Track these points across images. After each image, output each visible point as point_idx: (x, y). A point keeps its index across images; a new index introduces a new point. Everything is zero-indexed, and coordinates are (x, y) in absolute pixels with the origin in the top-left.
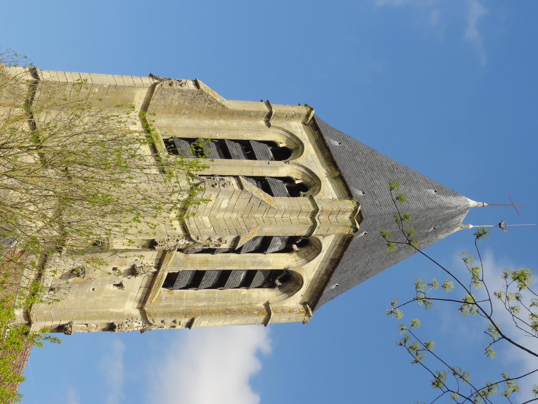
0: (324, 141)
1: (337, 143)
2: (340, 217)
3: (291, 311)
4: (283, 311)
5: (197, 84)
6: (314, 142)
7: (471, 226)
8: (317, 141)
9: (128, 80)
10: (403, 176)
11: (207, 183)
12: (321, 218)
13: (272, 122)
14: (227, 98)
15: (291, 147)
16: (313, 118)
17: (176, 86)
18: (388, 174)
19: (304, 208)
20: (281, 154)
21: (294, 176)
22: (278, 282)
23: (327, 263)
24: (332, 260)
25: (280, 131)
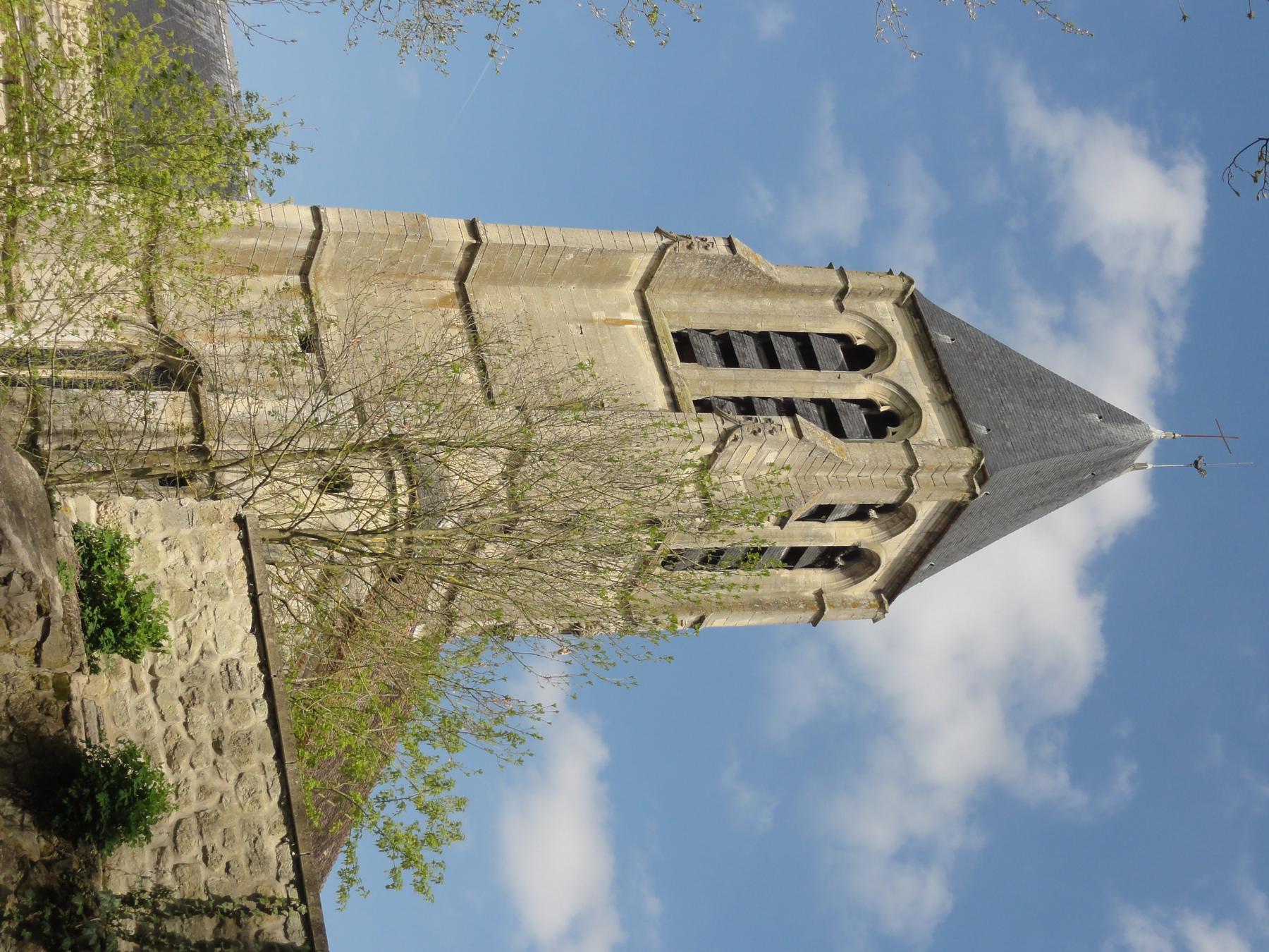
0: (928, 337)
2: (951, 474)
4: (844, 604)
5: (731, 246)
6: (911, 338)
8: (916, 336)
9: (620, 240)
10: (1050, 391)
11: (745, 428)
12: (921, 476)
13: (846, 302)
15: (875, 345)
16: (912, 295)
17: (698, 250)
20: (859, 357)
21: (878, 399)
22: (840, 561)
23: (921, 538)
24: (929, 534)
25: (859, 319)
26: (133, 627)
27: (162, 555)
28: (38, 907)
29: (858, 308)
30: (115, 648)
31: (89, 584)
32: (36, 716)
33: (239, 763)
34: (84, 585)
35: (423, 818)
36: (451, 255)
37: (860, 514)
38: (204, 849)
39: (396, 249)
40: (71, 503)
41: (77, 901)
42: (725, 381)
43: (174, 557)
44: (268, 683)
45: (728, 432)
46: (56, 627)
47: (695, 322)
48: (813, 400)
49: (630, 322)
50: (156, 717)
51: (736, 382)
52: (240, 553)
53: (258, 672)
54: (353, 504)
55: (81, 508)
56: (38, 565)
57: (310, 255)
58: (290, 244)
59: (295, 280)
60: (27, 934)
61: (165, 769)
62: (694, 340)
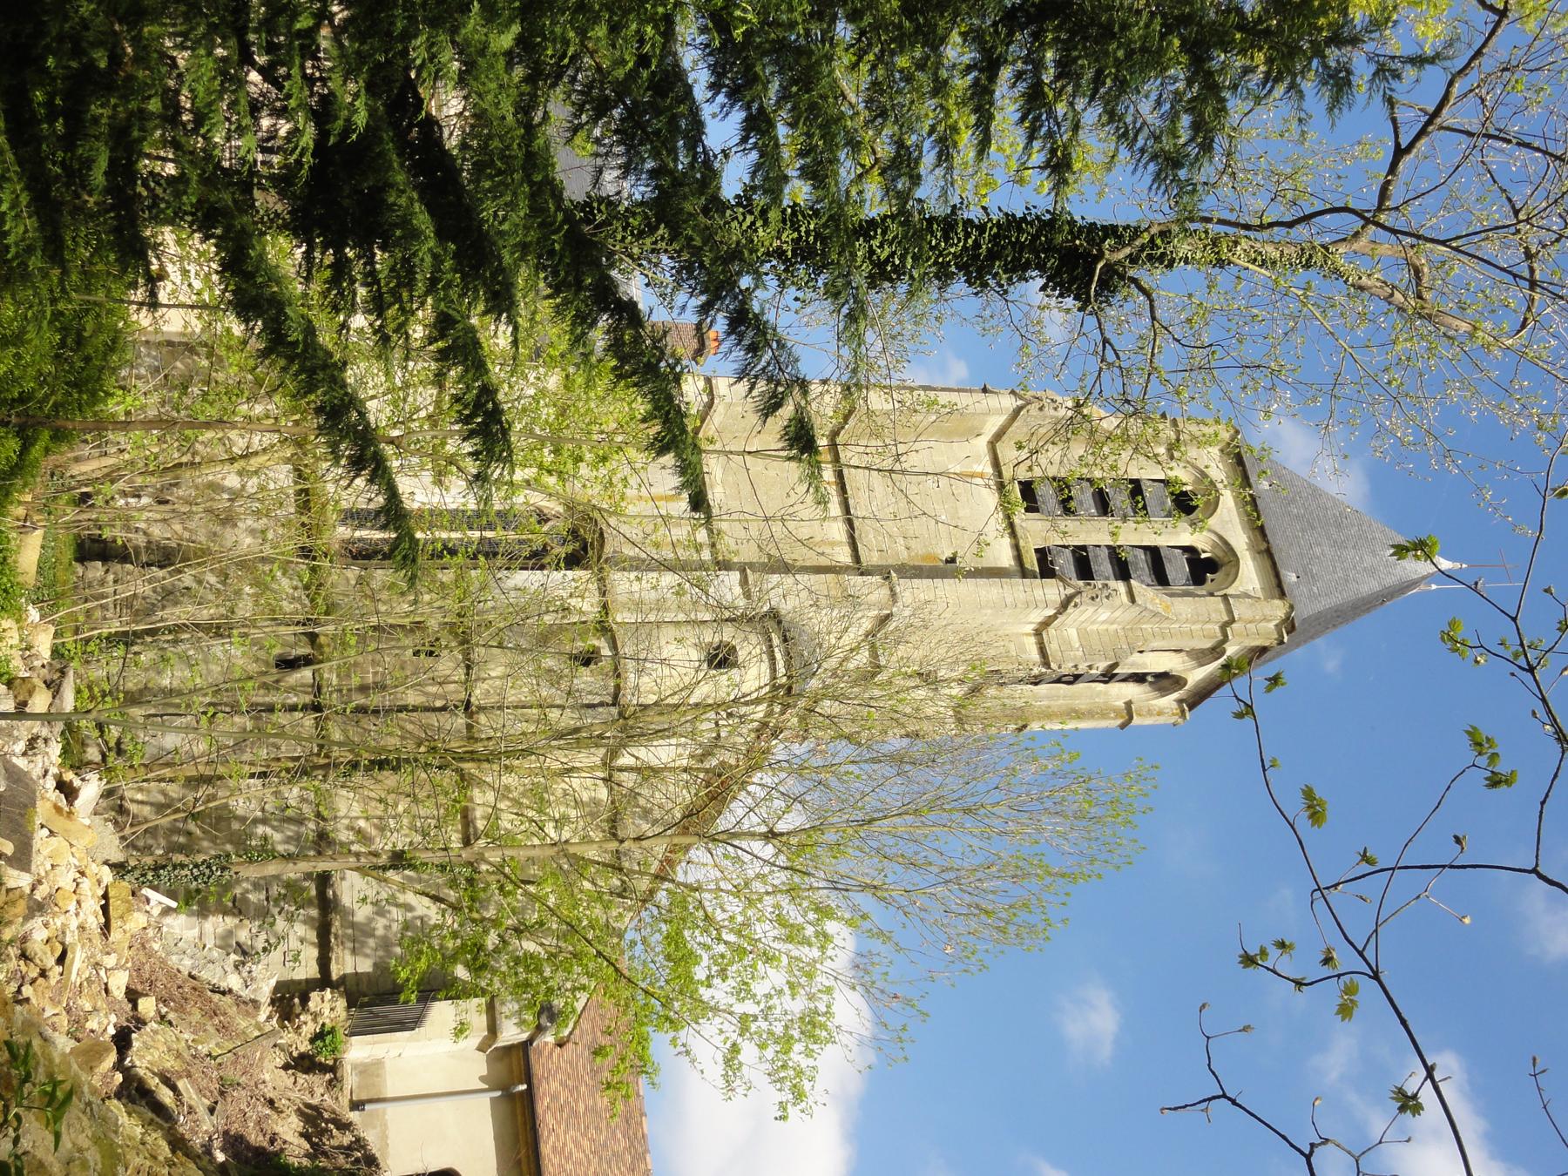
1: (1294, 579)
7: (1434, 587)
18: (1333, 530)
20: (1184, 504)
21: (1200, 546)
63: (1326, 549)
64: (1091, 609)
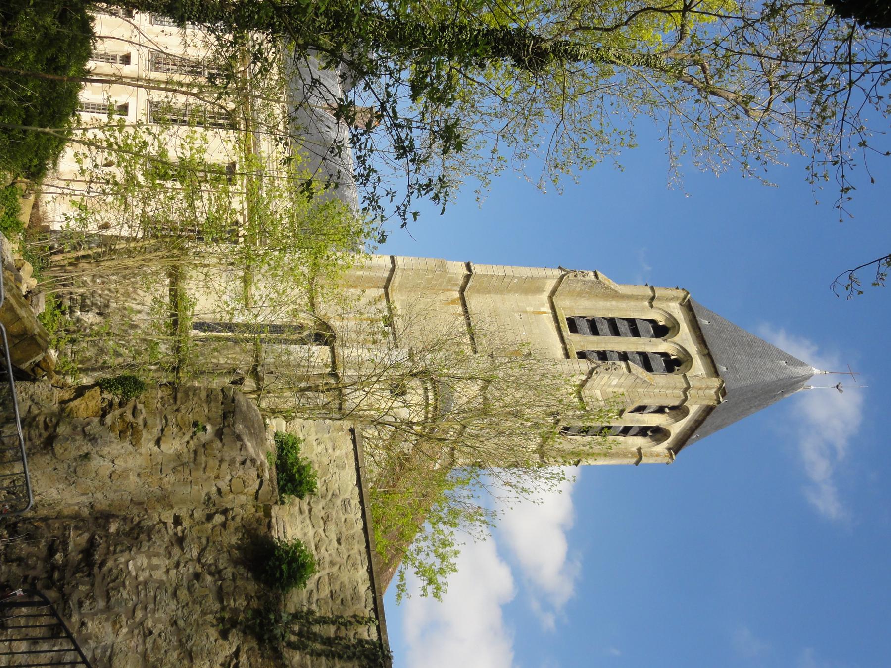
0: (697, 321)
1: (706, 322)
2: (707, 391)
3: (658, 455)
4: (652, 455)
5: (596, 275)
8: (691, 321)
12: (691, 393)
13: (654, 303)
14: (619, 283)
15: (669, 325)
17: (580, 277)
19: (678, 385)
20: (661, 331)
21: (670, 352)
22: (649, 433)
24: (696, 421)
25: (661, 312)
26: (301, 483)
27: (315, 447)
28: (254, 618)
29: (661, 306)
30: (292, 492)
31: (281, 462)
32: (255, 525)
33: (349, 550)
34: (279, 462)
35: (438, 561)
36: (457, 279)
37: (660, 410)
38: (331, 592)
39: (430, 276)
40: (274, 421)
41: (272, 616)
42: (592, 343)
43: (321, 448)
44: (363, 511)
45: (593, 369)
46: (265, 485)
47: (578, 313)
48: (638, 353)
49: (545, 313)
50: (310, 526)
51: (598, 343)
52: (352, 446)
53: (359, 505)
54: (407, 405)
55: (277, 425)
56: (258, 455)
57: (389, 280)
58: (379, 274)
59: (382, 291)
60: (248, 632)
61: (314, 552)
62: (577, 322)
63: (744, 357)
64: (607, 376)
